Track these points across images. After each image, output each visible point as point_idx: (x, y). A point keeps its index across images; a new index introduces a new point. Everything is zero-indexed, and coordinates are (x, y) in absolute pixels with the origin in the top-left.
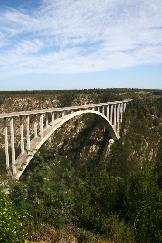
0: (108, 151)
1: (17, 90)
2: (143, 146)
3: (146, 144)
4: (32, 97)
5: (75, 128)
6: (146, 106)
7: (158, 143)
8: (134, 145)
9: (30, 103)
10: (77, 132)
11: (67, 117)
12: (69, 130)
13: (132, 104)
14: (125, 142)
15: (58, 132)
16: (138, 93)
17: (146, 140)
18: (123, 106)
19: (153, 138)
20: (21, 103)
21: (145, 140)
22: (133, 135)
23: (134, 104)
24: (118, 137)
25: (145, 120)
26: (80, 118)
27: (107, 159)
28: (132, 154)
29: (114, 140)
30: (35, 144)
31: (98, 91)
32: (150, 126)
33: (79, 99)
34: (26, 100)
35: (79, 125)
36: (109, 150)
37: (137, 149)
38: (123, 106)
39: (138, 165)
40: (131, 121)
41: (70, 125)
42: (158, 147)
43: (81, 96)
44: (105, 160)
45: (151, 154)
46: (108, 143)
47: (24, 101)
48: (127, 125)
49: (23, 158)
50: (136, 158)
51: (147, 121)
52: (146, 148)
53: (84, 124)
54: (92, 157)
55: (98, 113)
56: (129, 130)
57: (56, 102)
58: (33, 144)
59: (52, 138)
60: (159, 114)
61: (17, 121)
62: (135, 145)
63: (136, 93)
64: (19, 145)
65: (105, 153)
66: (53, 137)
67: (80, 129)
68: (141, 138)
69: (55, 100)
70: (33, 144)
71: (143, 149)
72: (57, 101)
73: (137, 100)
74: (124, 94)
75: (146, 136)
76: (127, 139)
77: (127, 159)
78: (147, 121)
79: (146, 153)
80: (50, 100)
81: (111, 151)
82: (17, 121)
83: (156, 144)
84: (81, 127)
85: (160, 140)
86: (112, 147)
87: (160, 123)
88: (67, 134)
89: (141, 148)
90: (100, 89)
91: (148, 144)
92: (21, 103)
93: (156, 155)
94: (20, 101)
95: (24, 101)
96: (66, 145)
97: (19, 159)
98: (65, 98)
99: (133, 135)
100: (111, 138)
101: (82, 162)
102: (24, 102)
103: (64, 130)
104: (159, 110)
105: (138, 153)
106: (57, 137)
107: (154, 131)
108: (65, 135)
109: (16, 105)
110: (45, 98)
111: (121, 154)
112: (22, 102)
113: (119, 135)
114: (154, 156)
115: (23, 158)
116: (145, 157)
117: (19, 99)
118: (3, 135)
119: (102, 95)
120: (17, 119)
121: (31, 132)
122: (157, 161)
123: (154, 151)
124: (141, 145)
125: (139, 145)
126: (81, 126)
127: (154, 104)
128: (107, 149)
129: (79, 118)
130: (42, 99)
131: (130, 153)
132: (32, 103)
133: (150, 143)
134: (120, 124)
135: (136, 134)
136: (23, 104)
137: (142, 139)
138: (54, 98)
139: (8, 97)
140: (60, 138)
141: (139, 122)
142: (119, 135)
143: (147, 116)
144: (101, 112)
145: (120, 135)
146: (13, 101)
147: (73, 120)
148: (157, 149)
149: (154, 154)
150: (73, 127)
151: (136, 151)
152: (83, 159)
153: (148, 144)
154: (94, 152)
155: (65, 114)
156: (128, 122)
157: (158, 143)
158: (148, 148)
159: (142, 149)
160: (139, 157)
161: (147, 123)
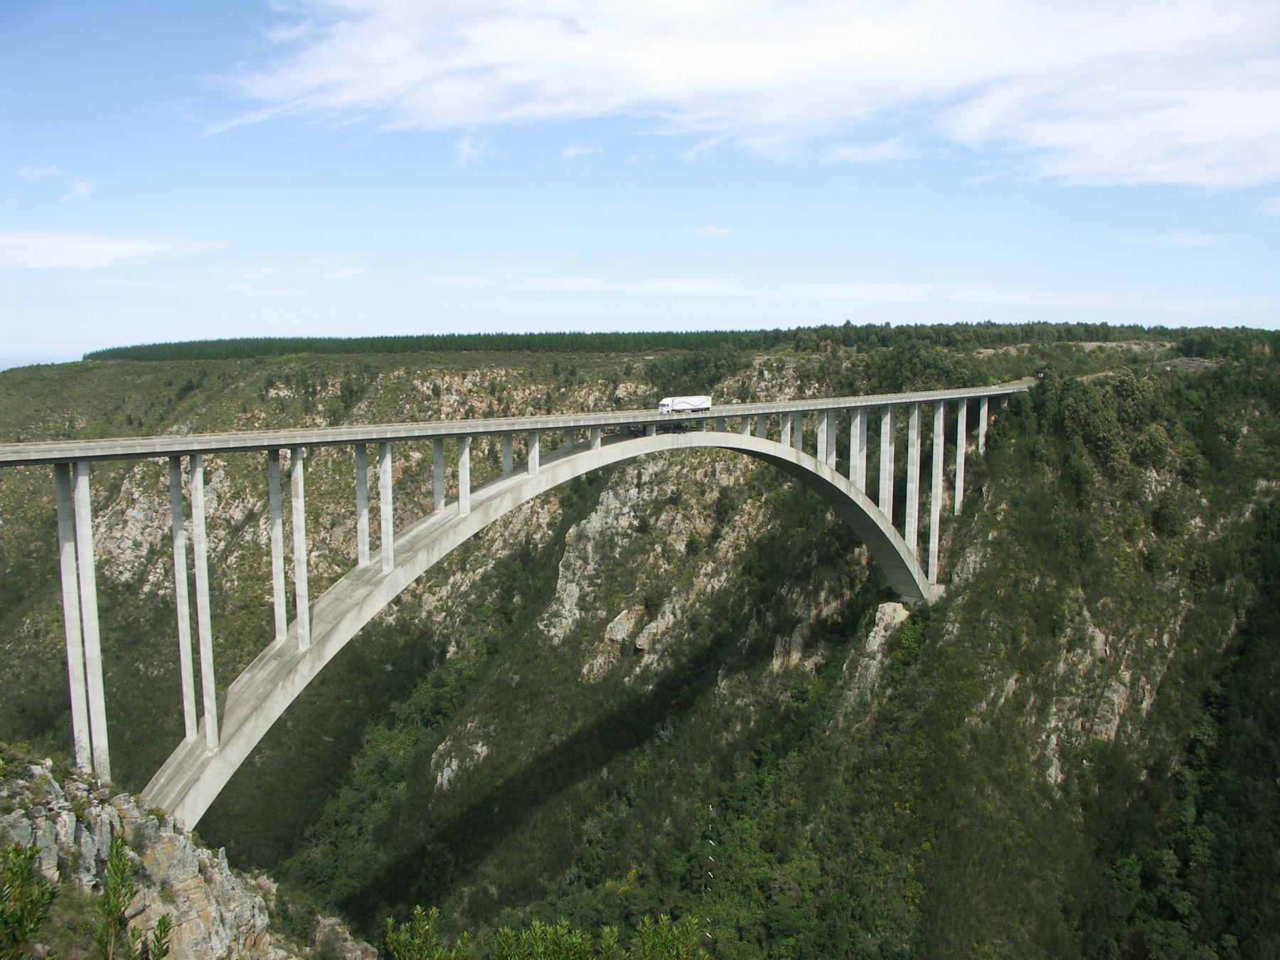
0: (867, 668)
1: (510, 333)
2: (1070, 649)
3: (1092, 639)
4: (514, 366)
5: (716, 536)
6: (1107, 422)
7: (1166, 637)
8: (1015, 640)
9: (500, 400)
10: (720, 554)
11: (561, 464)
12: (681, 547)
13: (1028, 407)
14: (965, 622)
15: (618, 550)
16: (1100, 348)
17: (1094, 615)
18: (973, 422)
19: (1136, 602)
20: (455, 397)
21: (1086, 613)
22: (1016, 584)
23: (1039, 408)
24: (933, 591)
25: (1102, 501)
26: (742, 480)
27: (855, 713)
28: (1001, 689)
29: (905, 605)
30: (348, 601)
31: (850, 336)
32: (1129, 535)
33: (750, 378)
34: (482, 382)
35: (737, 518)
36: (874, 665)
37: (1030, 663)
38: (973, 422)
39: (1033, 758)
40: (1015, 504)
41: (685, 517)
42: (1163, 657)
43: (759, 360)
44: (845, 716)
45: (1115, 698)
46: (873, 623)
47: (470, 386)
48: (989, 523)
49: (274, 664)
50: (1021, 714)
51: (1113, 504)
52: (1088, 659)
53: (764, 516)
54: (785, 697)
55: (784, 449)
56: (993, 555)
57: (635, 392)
58: (337, 599)
59: (585, 584)
60: (1188, 468)
61: (424, 489)
62: (1025, 639)
63: (1089, 346)
64: (424, 615)
65: (852, 676)
66: (591, 578)
67: (742, 542)
68: (1061, 600)
69: (631, 386)
70: (337, 599)
71: (1072, 667)
72: (640, 392)
73: (1058, 382)
74: (1006, 354)
75: (1093, 589)
76: (973, 607)
77: (961, 718)
78: (1113, 504)
79: (1087, 691)
80: (606, 387)
81: (884, 671)
82: (424, 489)
83: (1151, 642)
84: (743, 532)
85: (1186, 619)
86: (892, 645)
87: (1193, 517)
88: (664, 566)
89: (1057, 662)
90: (893, 326)
91: (1100, 638)
92: (455, 397)
93: (1145, 705)
94: (448, 390)
95: (470, 386)
96: (653, 624)
97: (256, 670)
98: (685, 372)
99: (1016, 584)
100: (891, 596)
101: (727, 724)
102: (470, 391)
103: (653, 544)
104: (1192, 444)
105: (1037, 689)
106: (611, 578)
107: (1149, 563)
108: (653, 573)
109: (429, 409)
110: (581, 372)
111: (933, 689)
112: (459, 392)
113: (939, 581)
114: (1138, 711)
115: (274, 664)
116: (1078, 716)
117: (447, 378)
118: (353, 556)
119: (877, 359)
120: (425, 482)
121: (493, 550)
122: (1152, 741)
123: (1135, 681)
124: (1063, 641)
125: (1049, 643)
126: (746, 527)
127: (1168, 410)
128: (862, 653)
129: (737, 479)
130: (562, 377)
131: (985, 686)
132: (510, 397)
133: (1116, 632)
134: (944, 521)
135: (1037, 580)
136: (463, 404)
137: (1067, 608)
138: (628, 372)
139: (395, 366)
140: (627, 587)
141: (1062, 511)
142: (939, 581)
143: (1110, 475)
144: (810, 446)
145: (944, 579)
146: (414, 388)
147: (703, 493)
148: (1159, 670)
149: (1135, 701)
150: (704, 527)
151: (1023, 673)
152: (732, 703)
153: (1100, 638)
154: (796, 667)
155: (541, 457)
156: (992, 507)
157: (1166, 637)
158: (1102, 661)
159: (1061, 668)
160: (1042, 712)
161: (1107, 517)
